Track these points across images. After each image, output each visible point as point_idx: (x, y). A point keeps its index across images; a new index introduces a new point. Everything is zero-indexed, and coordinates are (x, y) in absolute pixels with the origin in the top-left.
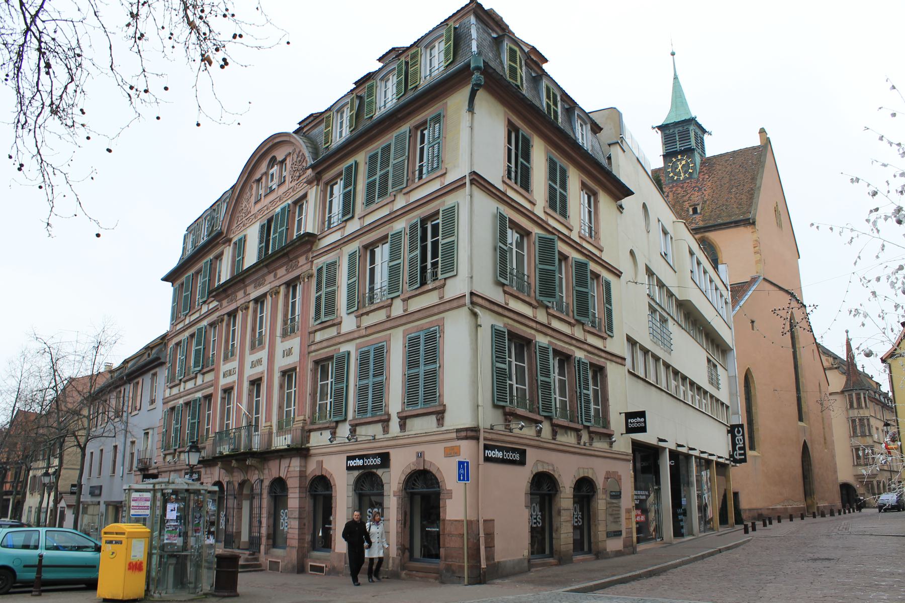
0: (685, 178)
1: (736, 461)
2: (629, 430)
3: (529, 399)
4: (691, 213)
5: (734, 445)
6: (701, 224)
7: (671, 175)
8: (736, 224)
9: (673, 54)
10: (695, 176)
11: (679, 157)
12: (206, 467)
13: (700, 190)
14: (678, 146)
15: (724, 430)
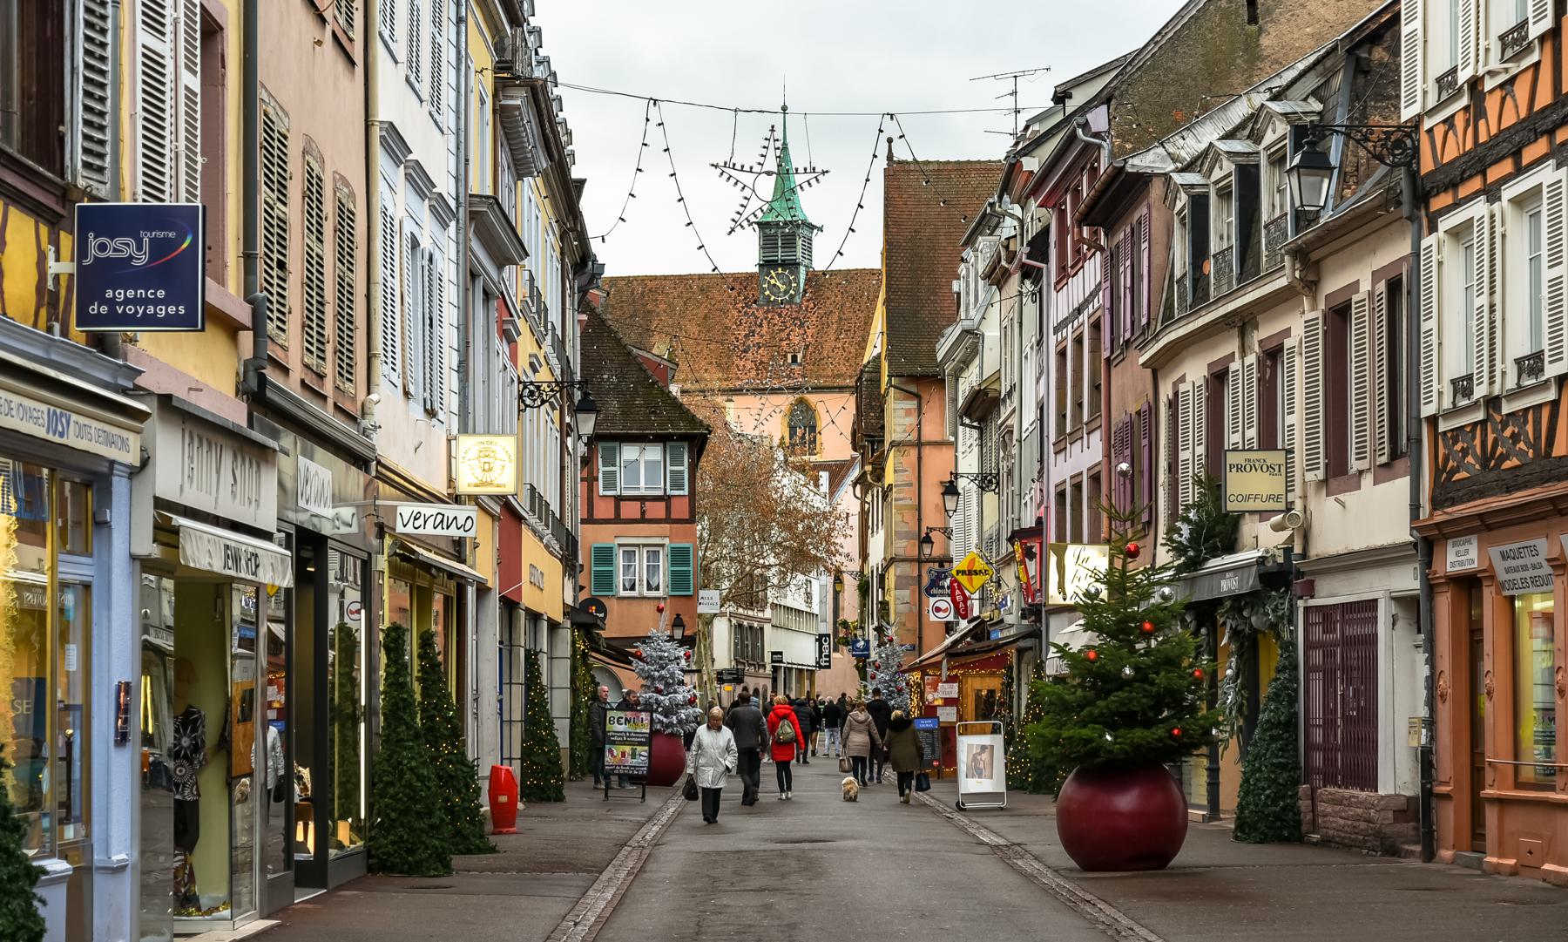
1: (821, 667)
2: (773, 661)
4: (789, 361)
5: (821, 652)
7: (767, 293)
10: (797, 300)
11: (780, 270)
13: (802, 325)
14: (780, 255)
15: (813, 638)
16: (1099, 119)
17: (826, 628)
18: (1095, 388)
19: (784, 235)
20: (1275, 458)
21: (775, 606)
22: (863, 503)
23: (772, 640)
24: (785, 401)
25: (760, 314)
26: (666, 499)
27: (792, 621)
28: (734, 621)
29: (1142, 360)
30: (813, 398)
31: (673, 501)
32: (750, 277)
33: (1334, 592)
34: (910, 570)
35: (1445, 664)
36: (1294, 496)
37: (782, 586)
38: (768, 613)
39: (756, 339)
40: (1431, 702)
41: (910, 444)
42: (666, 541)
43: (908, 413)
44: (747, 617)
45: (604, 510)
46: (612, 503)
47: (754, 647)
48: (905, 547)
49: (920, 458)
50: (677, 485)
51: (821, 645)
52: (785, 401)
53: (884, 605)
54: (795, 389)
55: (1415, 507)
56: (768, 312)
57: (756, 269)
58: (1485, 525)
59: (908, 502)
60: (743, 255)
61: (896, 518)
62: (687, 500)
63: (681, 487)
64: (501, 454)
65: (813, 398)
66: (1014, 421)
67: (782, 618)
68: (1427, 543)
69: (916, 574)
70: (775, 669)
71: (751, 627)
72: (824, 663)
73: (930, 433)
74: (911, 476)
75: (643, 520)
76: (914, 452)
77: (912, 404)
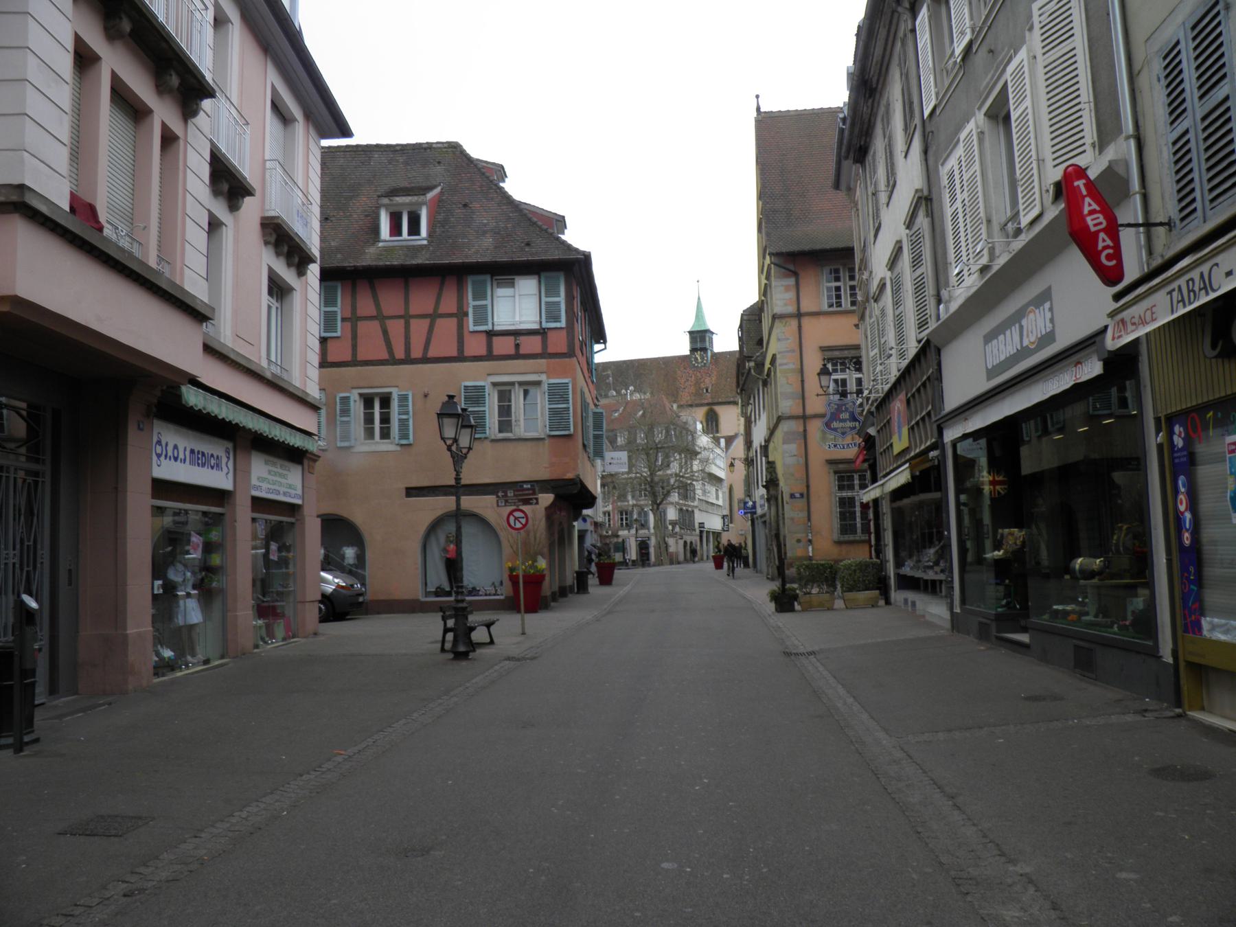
3: (870, 521)
5: (724, 523)
6: (710, 401)
14: (699, 346)
15: (720, 518)
17: (726, 512)
23: (699, 517)
27: (710, 508)
28: (678, 507)
30: (717, 408)
31: (550, 334)
32: (687, 356)
38: (696, 503)
39: (689, 383)
42: (543, 377)
43: (787, 288)
44: (685, 505)
45: (475, 346)
46: (483, 338)
47: (690, 520)
49: (800, 327)
50: (553, 316)
52: (703, 410)
54: (708, 404)
59: (792, 366)
62: (564, 333)
63: (557, 319)
65: (717, 408)
67: (704, 506)
69: (801, 429)
70: (701, 532)
71: (687, 510)
73: (807, 306)
74: (792, 342)
75: (517, 356)
76: (794, 323)
77: (791, 281)
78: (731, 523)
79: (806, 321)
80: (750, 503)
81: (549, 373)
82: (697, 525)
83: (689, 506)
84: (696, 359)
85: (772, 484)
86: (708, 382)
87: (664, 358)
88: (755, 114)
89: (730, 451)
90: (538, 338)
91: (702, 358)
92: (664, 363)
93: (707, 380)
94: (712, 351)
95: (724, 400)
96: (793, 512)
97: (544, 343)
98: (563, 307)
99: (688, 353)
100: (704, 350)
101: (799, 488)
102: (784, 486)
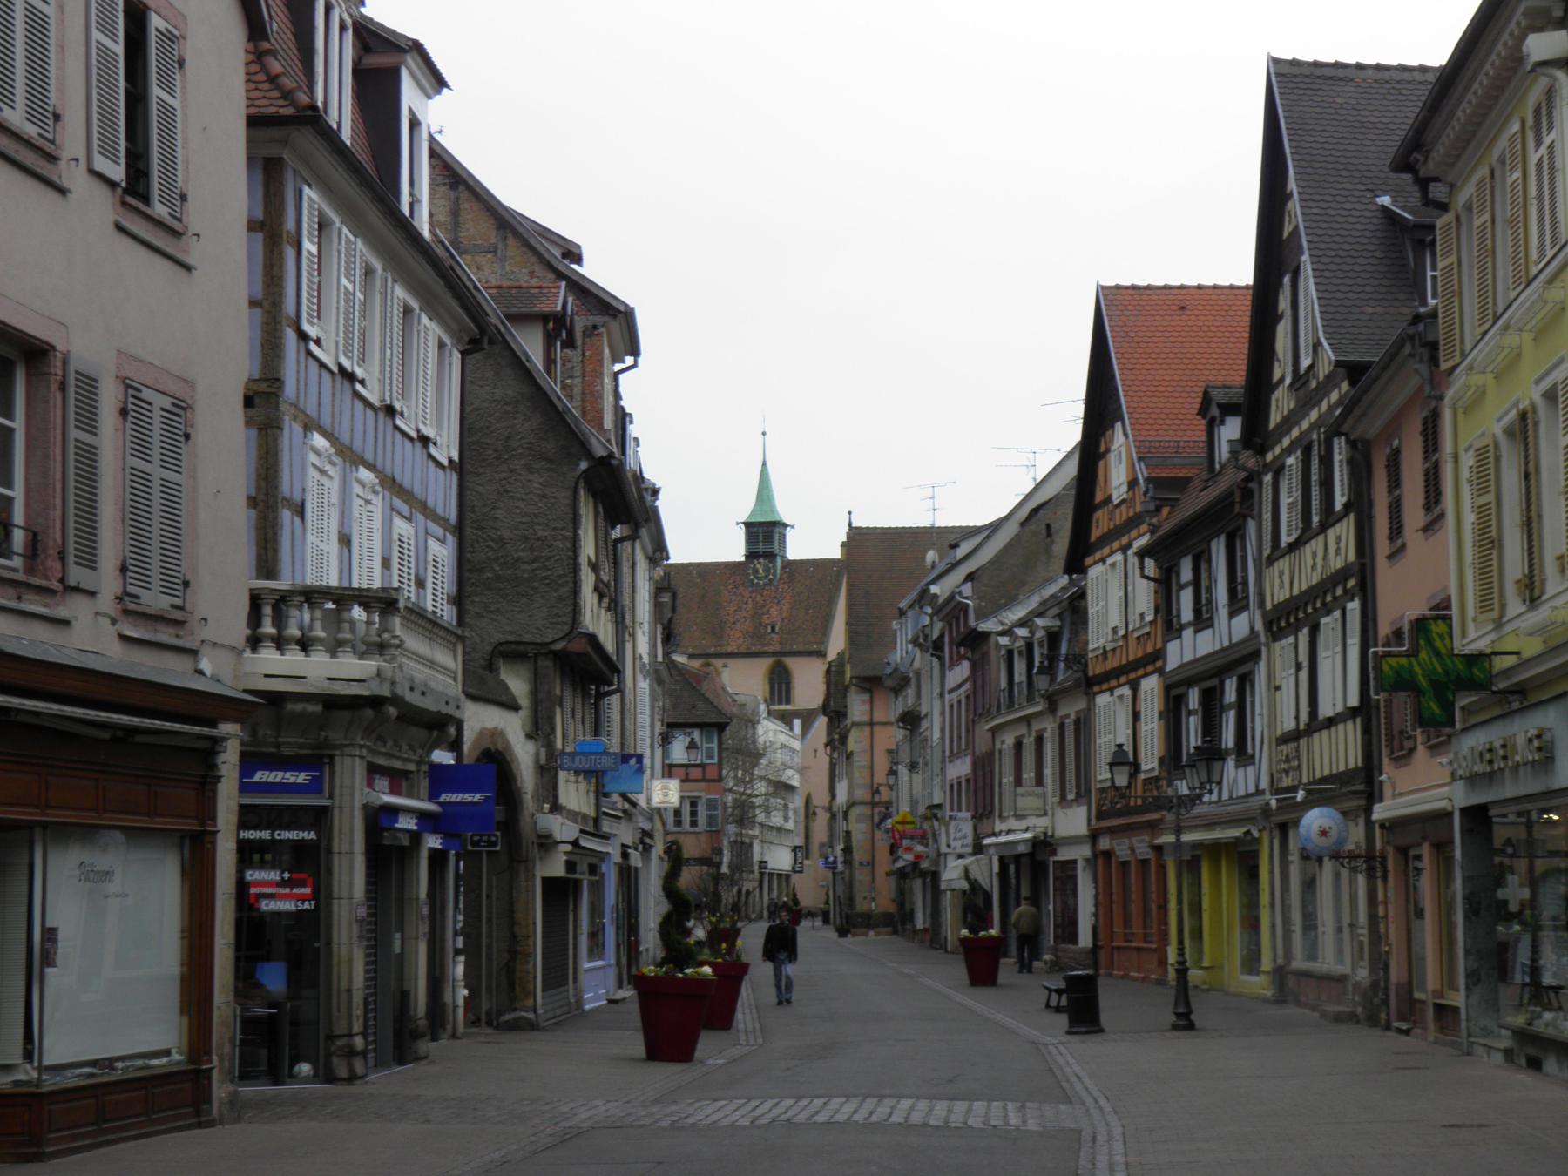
0: (765, 584)
5: (795, 860)
6: (777, 648)
8: (810, 653)
9: (764, 434)
10: (775, 583)
12: (1245, 766)
14: (761, 548)
15: (789, 850)
16: (967, 589)
17: (799, 841)
18: (968, 731)
19: (764, 532)
20: (1039, 790)
21: (761, 825)
22: (831, 758)
24: (766, 663)
25: (746, 594)
26: (702, 766)
29: (987, 727)
33: (1064, 854)
34: (866, 810)
35: (1101, 890)
36: (1048, 808)
37: (767, 810)
39: (744, 614)
40: (1096, 905)
41: (864, 724)
42: (702, 794)
43: (863, 702)
48: (861, 794)
51: (796, 855)
52: (766, 663)
53: (848, 833)
54: (774, 654)
55: (1089, 820)
56: (752, 592)
57: (743, 559)
58: (1111, 831)
60: (734, 550)
61: (856, 774)
63: (712, 758)
64: (672, 786)
66: (927, 733)
68: (1094, 836)
69: (869, 812)
70: (762, 874)
72: (797, 868)
74: (865, 745)
76: (867, 730)
77: (866, 697)
78: (807, 857)
79: (875, 720)
80: (831, 859)
81: (708, 791)
82: (756, 868)
83: (747, 835)
84: (756, 571)
85: (848, 850)
86: (775, 614)
87: (699, 565)
88: (846, 529)
89: (809, 736)
90: (700, 769)
91: (767, 570)
92: (700, 575)
93: (774, 612)
94: (783, 557)
95: (801, 648)
96: (861, 876)
97: (704, 773)
98: (716, 750)
99: (743, 559)
100: (771, 556)
101: (867, 858)
102: (858, 855)
